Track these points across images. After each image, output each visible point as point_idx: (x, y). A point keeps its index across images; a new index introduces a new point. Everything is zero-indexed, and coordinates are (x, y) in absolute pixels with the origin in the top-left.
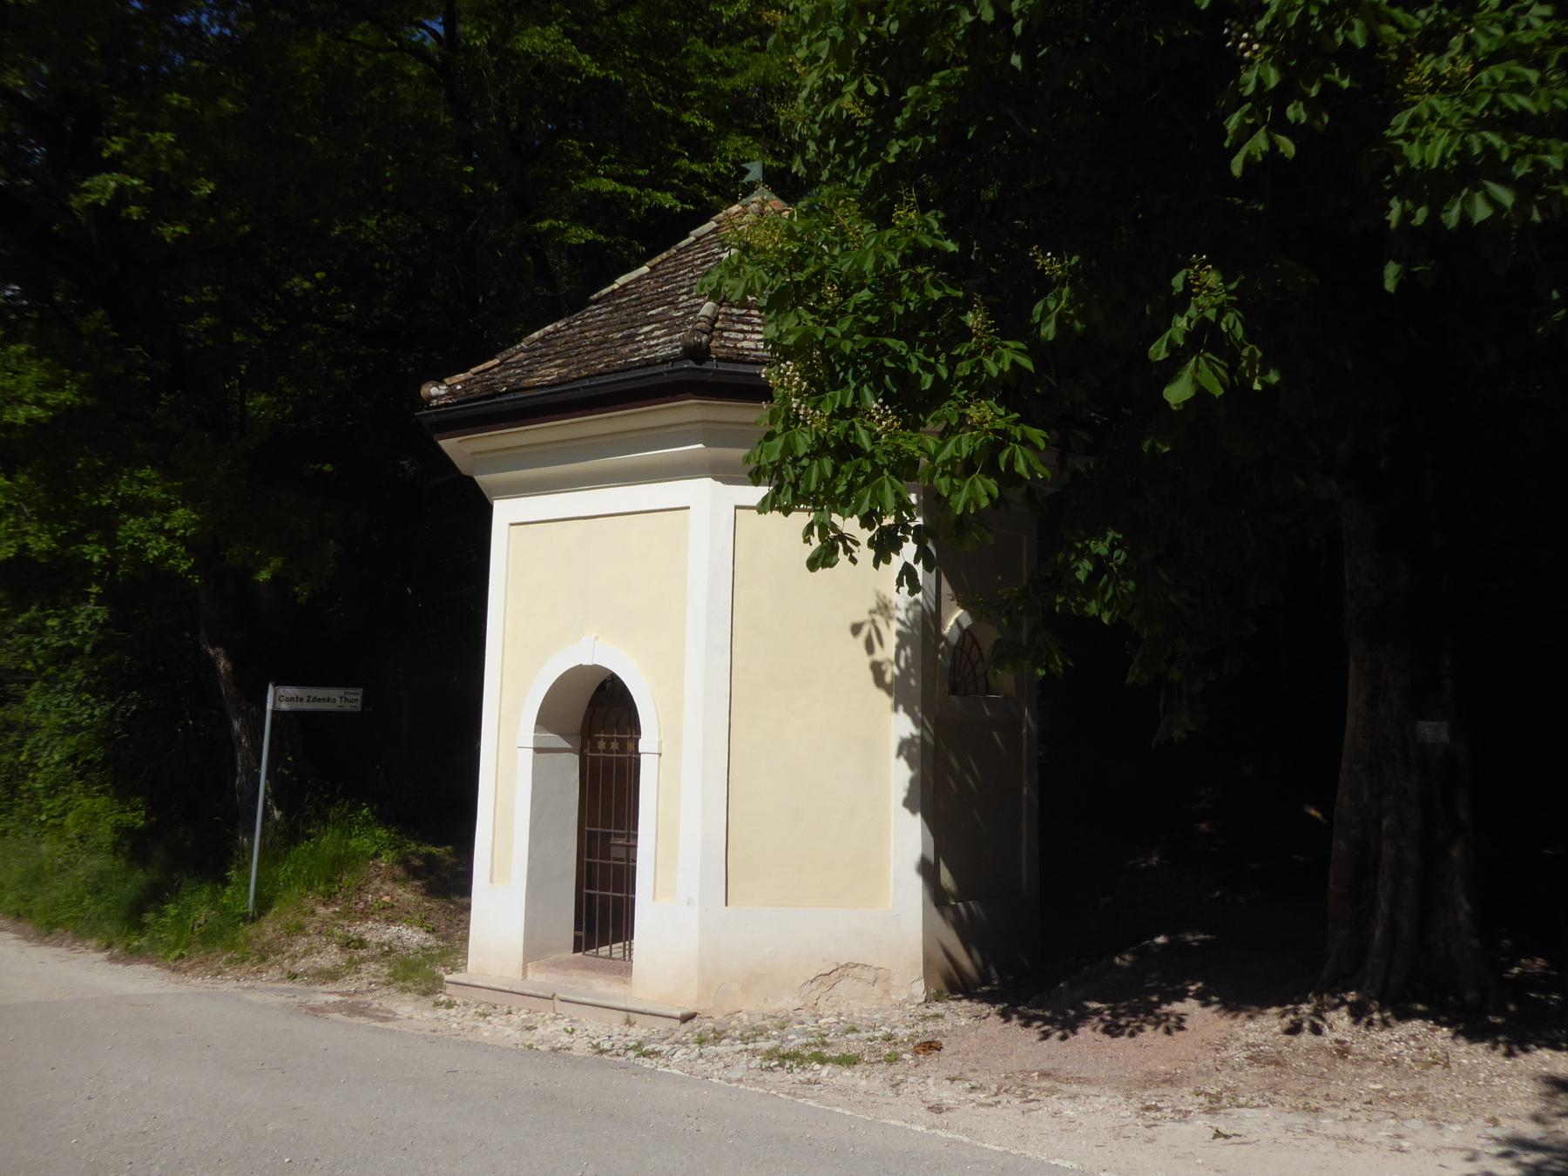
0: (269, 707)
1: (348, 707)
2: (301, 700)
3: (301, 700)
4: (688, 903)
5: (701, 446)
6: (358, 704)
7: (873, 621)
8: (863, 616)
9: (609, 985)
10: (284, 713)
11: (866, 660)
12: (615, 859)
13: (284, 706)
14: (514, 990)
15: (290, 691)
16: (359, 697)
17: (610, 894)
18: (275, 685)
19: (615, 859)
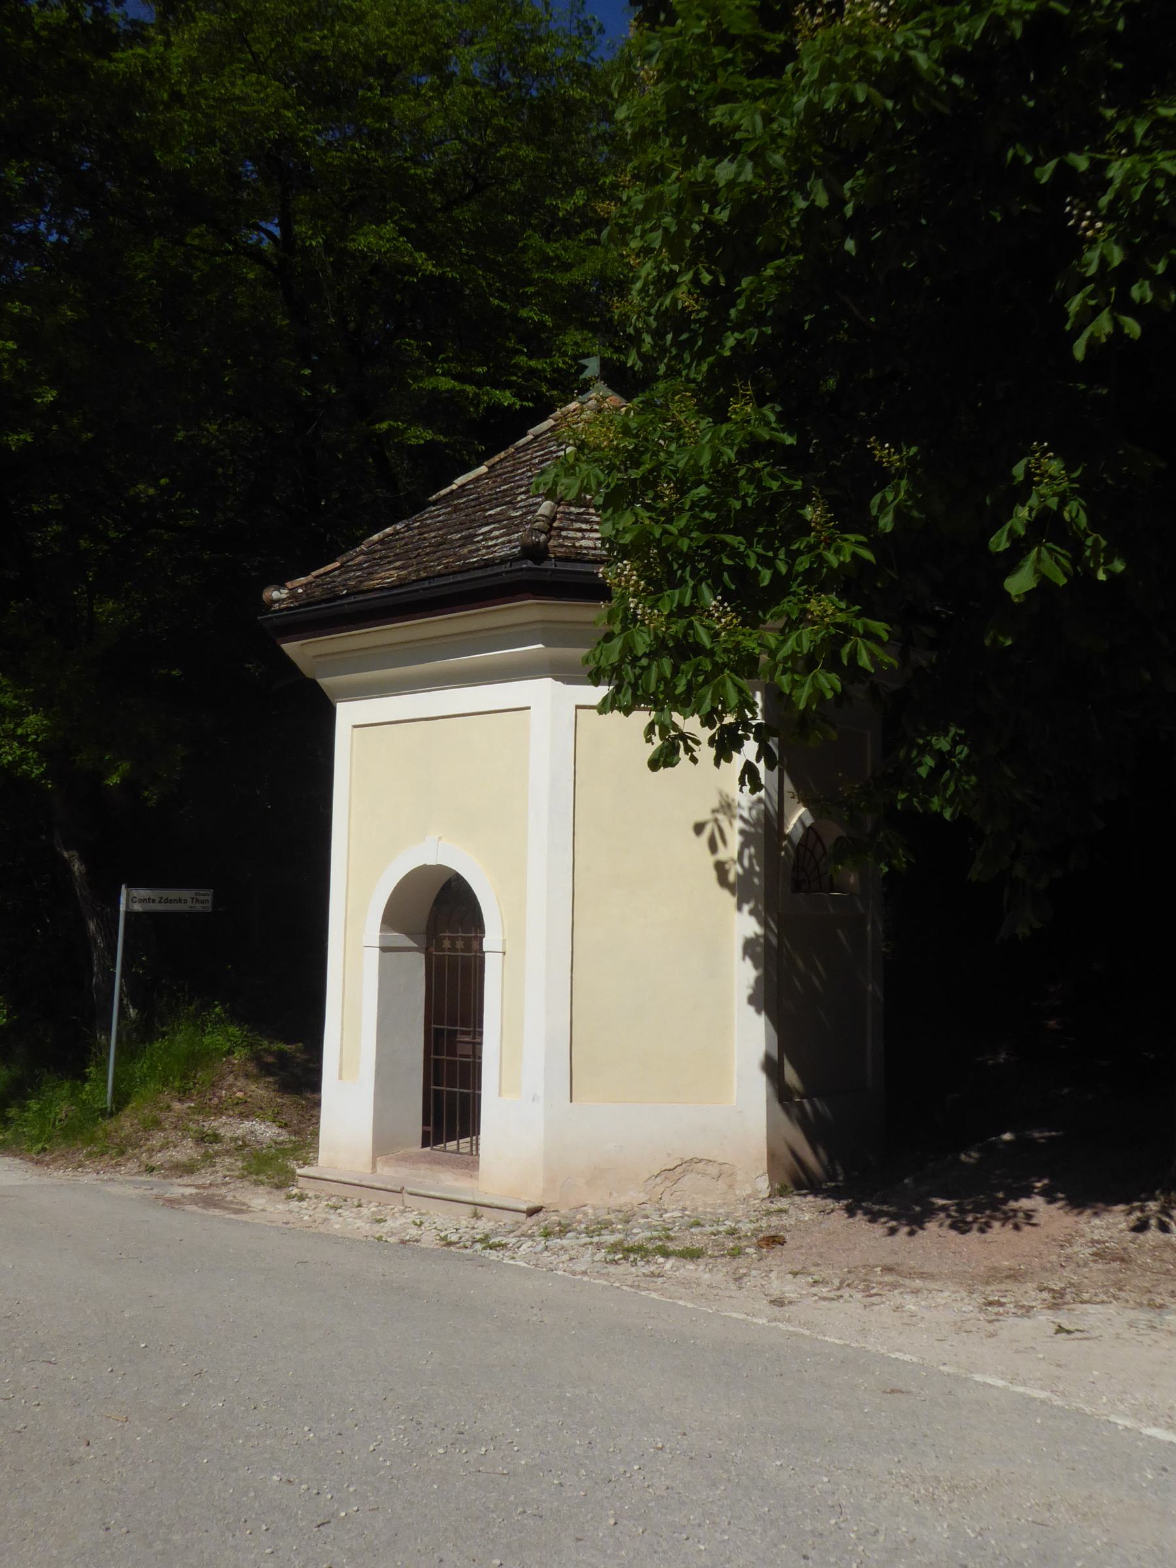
0: (122, 908)
1: (199, 907)
2: (153, 901)
3: (153, 901)
4: (534, 1099)
5: (540, 646)
6: (209, 905)
7: (716, 820)
8: (704, 815)
9: (456, 1179)
10: (137, 914)
11: (710, 860)
12: (461, 1056)
13: (137, 907)
14: (364, 1183)
15: (142, 893)
16: (210, 898)
17: (456, 1090)
18: (128, 886)
19: (461, 1056)
